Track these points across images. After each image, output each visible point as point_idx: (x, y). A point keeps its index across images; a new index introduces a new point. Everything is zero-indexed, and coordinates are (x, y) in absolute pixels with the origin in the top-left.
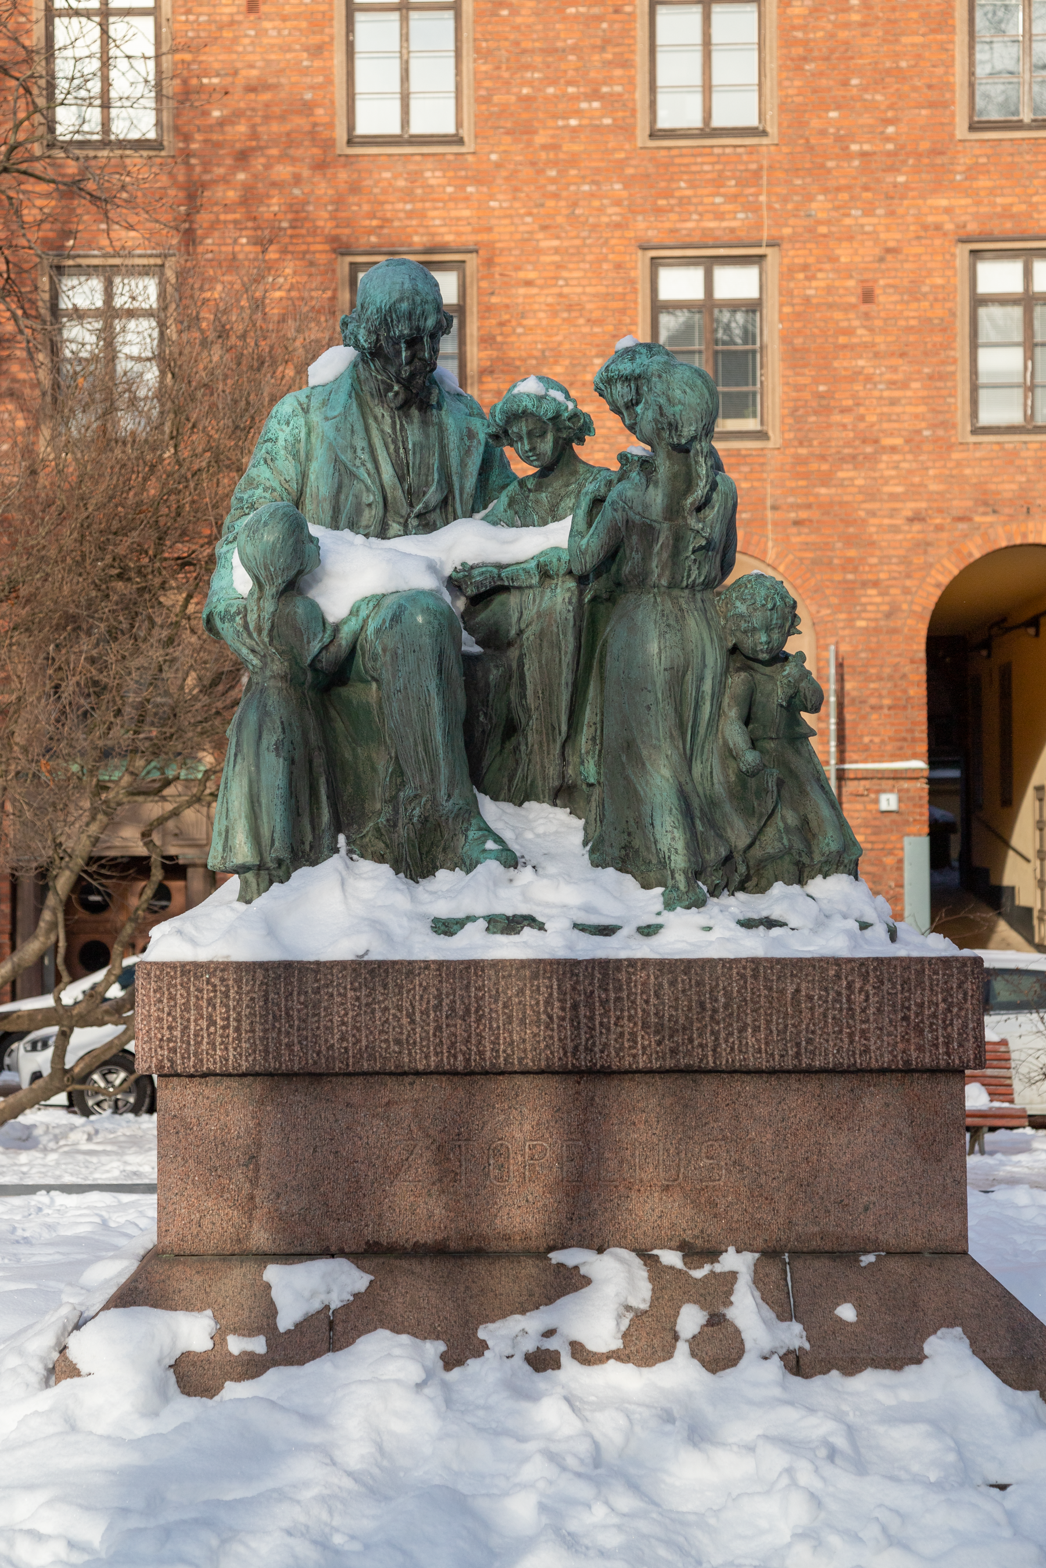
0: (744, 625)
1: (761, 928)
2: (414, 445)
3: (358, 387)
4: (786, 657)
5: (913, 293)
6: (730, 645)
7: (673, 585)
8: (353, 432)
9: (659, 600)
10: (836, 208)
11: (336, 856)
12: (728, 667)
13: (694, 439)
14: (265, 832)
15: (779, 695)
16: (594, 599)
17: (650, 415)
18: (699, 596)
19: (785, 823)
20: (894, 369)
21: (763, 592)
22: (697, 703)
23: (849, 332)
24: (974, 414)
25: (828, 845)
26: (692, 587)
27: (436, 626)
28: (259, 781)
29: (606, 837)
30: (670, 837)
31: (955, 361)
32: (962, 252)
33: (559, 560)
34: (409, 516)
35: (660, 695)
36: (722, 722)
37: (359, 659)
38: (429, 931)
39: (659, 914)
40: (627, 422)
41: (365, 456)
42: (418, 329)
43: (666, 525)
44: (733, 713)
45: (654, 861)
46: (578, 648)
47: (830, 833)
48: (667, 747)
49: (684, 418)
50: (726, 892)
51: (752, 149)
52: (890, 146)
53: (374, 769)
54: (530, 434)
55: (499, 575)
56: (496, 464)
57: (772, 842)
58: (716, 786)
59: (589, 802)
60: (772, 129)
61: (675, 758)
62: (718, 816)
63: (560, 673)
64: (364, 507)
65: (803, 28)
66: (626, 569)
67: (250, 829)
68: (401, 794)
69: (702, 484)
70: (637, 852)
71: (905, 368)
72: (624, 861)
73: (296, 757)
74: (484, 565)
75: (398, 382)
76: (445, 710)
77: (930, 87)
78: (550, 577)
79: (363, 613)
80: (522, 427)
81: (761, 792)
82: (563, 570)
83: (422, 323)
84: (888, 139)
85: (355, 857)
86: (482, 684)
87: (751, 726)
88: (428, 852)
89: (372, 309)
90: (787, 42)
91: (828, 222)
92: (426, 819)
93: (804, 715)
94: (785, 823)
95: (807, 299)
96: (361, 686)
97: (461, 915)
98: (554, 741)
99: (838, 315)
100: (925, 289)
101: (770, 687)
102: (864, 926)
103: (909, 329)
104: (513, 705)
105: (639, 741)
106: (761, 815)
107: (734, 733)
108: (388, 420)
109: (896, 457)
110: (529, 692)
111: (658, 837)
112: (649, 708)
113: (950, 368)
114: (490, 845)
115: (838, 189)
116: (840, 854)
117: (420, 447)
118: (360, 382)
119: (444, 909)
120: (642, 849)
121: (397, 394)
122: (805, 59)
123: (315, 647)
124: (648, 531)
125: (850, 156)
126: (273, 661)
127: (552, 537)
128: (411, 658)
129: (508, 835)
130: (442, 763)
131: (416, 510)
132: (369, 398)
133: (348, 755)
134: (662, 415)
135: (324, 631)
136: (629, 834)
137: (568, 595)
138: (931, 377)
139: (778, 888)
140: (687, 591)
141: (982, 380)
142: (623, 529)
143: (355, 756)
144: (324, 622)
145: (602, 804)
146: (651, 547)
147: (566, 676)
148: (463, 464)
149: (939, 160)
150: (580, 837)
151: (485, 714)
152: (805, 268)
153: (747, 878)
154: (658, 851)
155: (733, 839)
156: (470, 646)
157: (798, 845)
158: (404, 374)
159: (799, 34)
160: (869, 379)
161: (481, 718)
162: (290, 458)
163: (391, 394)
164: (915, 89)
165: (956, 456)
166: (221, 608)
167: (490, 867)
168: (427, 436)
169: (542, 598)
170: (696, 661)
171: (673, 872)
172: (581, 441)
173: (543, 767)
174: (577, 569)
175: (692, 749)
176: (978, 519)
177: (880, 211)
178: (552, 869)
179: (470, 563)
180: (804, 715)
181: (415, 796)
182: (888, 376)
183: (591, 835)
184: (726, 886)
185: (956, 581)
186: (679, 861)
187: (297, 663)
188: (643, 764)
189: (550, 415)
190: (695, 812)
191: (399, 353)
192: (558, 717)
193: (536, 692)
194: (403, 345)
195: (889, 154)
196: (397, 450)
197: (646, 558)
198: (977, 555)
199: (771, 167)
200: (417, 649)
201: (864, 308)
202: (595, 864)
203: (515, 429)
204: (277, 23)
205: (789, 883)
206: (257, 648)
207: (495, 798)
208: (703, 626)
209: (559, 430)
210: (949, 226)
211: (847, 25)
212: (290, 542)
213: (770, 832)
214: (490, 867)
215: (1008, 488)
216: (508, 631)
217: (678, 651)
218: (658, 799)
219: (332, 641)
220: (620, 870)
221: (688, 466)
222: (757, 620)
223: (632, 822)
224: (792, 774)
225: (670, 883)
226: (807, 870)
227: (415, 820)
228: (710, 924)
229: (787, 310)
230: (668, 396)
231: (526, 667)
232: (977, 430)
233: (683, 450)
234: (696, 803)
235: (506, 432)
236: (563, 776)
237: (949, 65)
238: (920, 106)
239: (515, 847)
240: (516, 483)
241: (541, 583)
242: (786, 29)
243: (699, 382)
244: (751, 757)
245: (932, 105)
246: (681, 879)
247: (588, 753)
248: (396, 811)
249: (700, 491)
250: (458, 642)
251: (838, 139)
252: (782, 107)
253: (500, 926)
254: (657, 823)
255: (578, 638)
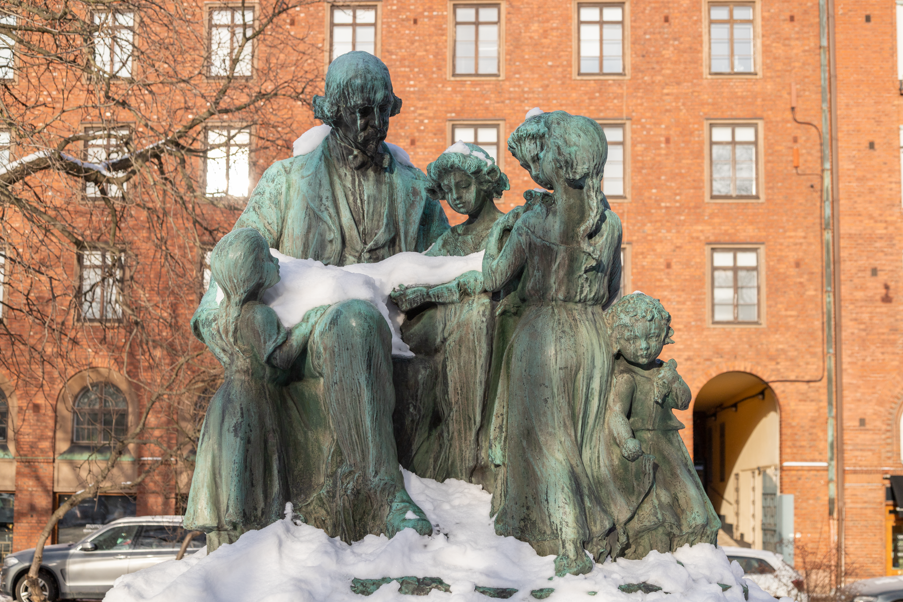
0: (627, 334)
1: (640, 592)
2: (369, 197)
3: (327, 153)
4: (660, 364)
5: (687, 265)
6: (615, 351)
7: (568, 299)
8: (320, 185)
9: (556, 311)
10: (655, 229)
11: (279, 521)
12: (613, 369)
13: (586, 176)
14: (224, 498)
15: (656, 394)
16: (504, 313)
17: (550, 156)
18: (590, 309)
19: (660, 501)
20: (679, 296)
21: (644, 306)
22: (587, 398)
23: (661, 280)
24: (713, 316)
25: (694, 519)
26: (584, 301)
27: (366, 328)
28: (220, 457)
29: (509, 511)
30: (563, 513)
31: (705, 294)
32: (708, 248)
33: (476, 280)
34: (363, 251)
35: (555, 390)
36: (607, 415)
37: (309, 358)
38: (348, 590)
39: (550, 579)
40: (534, 173)
41: (329, 203)
42: (369, 100)
43: (562, 247)
44: (616, 408)
45: (548, 532)
46: (490, 353)
47: (696, 509)
48: (561, 435)
49: (579, 158)
50: (609, 559)
51: (620, 204)
52: (678, 204)
53: (320, 449)
54: (457, 185)
55: (428, 293)
56: (436, 218)
57: (648, 515)
58: (603, 469)
59: (496, 480)
60: (629, 196)
61: (568, 444)
62: (603, 494)
63: (476, 373)
64: (327, 243)
65: (642, 156)
66: (529, 285)
67: (211, 497)
68: (339, 470)
69: (593, 214)
70: (534, 523)
71: (684, 296)
72: (523, 531)
73: (252, 438)
74: (417, 286)
75: (357, 148)
76: (373, 400)
77: (694, 181)
78: (468, 294)
79: (312, 320)
80: (450, 180)
81: (640, 474)
82: (479, 289)
83: (372, 95)
84: (677, 201)
85: (298, 522)
86: (412, 382)
87: (632, 419)
88: (361, 519)
89: (334, 85)
90: (635, 161)
91: (652, 235)
92: (358, 492)
93: (675, 412)
94: (660, 501)
95: (643, 267)
96: (312, 381)
97: (377, 576)
98: (470, 429)
99: (656, 273)
100: (692, 263)
101: (648, 387)
102: (725, 588)
103: (686, 280)
104: (438, 400)
105: (537, 429)
106: (640, 493)
107: (617, 424)
108: (349, 178)
109: (680, 333)
110: (451, 389)
111: (552, 511)
112: (546, 401)
113: (703, 297)
114: (410, 515)
115: (656, 221)
116: (704, 526)
117: (375, 199)
118: (329, 150)
119: (364, 570)
120: (538, 521)
121: (356, 157)
122: (642, 168)
123: (270, 346)
124: (547, 252)
125: (661, 208)
126: (238, 358)
127: (469, 266)
128: (345, 355)
129: (426, 507)
130: (371, 445)
131: (368, 247)
132: (336, 162)
133: (301, 438)
134: (559, 154)
135: (278, 333)
136: (528, 508)
137: (482, 308)
138: (695, 300)
139: (653, 556)
140: (580, 305)
141: (716, 301)
142: (527, 251)
143: (306, 438)
144: (279, 326)
145: (506, 482)
146: (549, 265)
147: (480, 376)
148: (408, 214)
149: (698, 211)
150: (487, 509)
151: (415, 407)
152: (642, 253)
153: (628, 546)
154: (551, 523)
155: (616, 514)
156: (400, 348)
157: (670, 519)
158: (360, 139)
159: (640, 158)
160: (669, 300)
161: (411, 410)
162: (273, 206)
163: (351, 157)
164: (688, 181)
165: (705, 333)
166: (203, 317)
167: (408, 534)
168: (380, 192)
169: (461, 311)
170: (586, 363)
171: (564, 543)
172: (500, 194)
173: (461, 450)
174: (489, 286)
175: (582, 437)
176: (715, 360)
177: (674, 231)
178: (461, 536)
179: (406, 285)
180: (675, 412)
181: (350, 472)
182: (677, 299)
183: (496, 508)
184: (610, 553)
185: (705, 386)
186: (570, 532)
187: (257, 360)
188: (541, 449)
189: (473, 169)
190: (583, 490)
191: (354, 122)
192: (474, 410)
193: (455, 389)
194: (358, 115)
195: (677, 208)
196: (355, 201)
197: (546, 275)
198: (714, 375)
199: (628, 212)
200: (350, 347)
201: (667, 270)
202: (499, 533)
203: (446, 182)
204: (423, 149)
205: (662, 551)
206: (227, 348)
207: (422, 475)
208: (593, 333)
209: (481, 183)
210: (702, 238)
211: (659, 155)
212: (250, 259)
213: (647, 508)
214: (408, 534)
215: (727, 347)
216: (435, 339)
217: (571, 353)
218: (552, 479)
219: (284, 342)
220: (520, 539)
221: (582, 200)
222: (639, 328)
223: (530, 498)
224: (665, 458)
225: (561, 551)
226: (677, 539)
227: (349, 492)
228: (595, 589)
229: (635, 271)
230: (565, 139)
231: (448, 369)
232: (714, 323)
233: (577, 185)
234: (584, 483)
235: (439, 186)
236: (477, 458)
237: (702, 172)
238: (690, 188)
239: (432, 518)
240: (449, 230)
241: (461, 300)
242: (634, 156)
243: (591, 129)
244: (632, 445)
245: (695, 188)
246: (571, 549)
247: (495, 439)
248: (335, 484)
249: (592, 220)
250: (388, 346)
251: (656, 201)
252: (633, 187)
253: (411, 587)
254: (551, 499)
255: (490, 345)
